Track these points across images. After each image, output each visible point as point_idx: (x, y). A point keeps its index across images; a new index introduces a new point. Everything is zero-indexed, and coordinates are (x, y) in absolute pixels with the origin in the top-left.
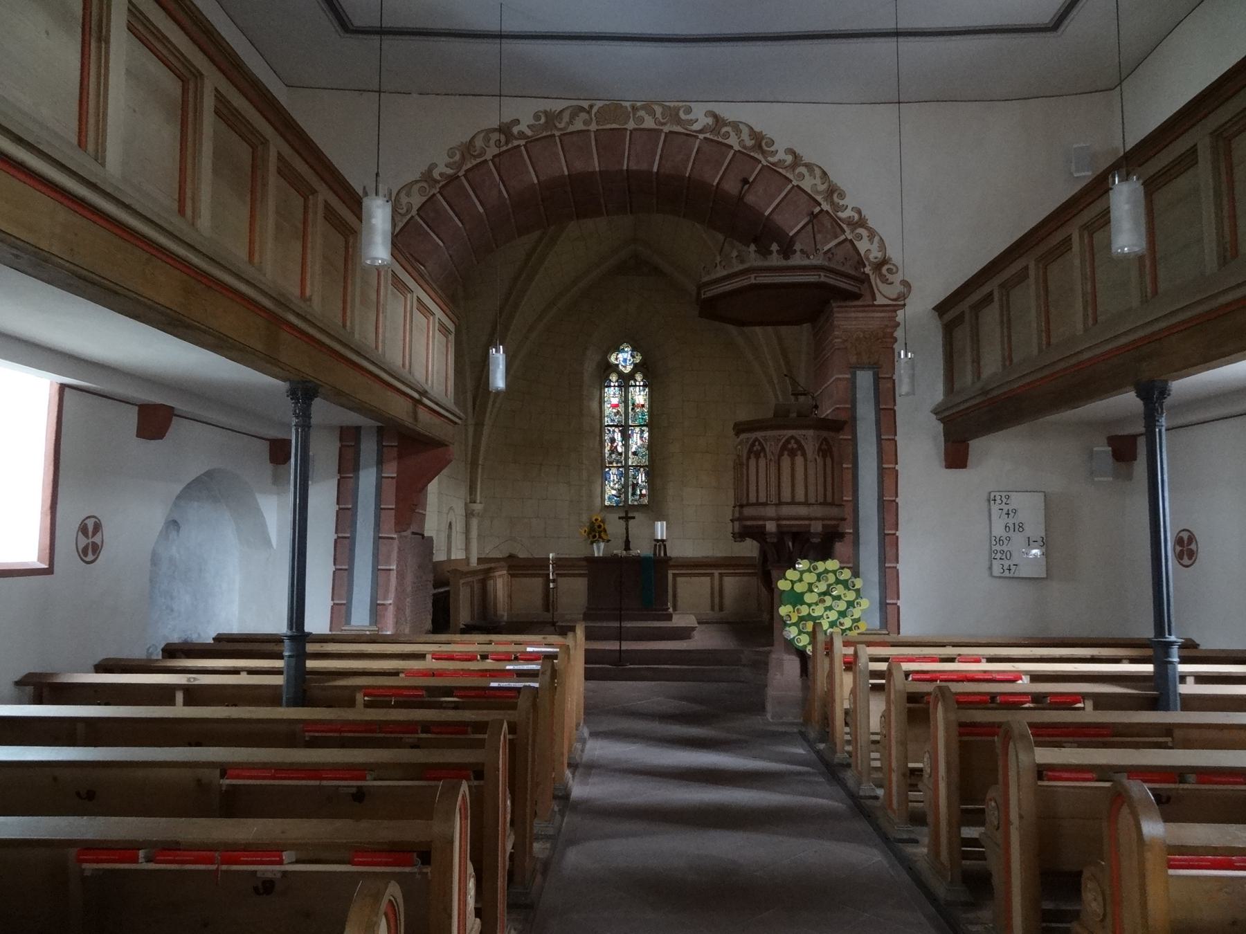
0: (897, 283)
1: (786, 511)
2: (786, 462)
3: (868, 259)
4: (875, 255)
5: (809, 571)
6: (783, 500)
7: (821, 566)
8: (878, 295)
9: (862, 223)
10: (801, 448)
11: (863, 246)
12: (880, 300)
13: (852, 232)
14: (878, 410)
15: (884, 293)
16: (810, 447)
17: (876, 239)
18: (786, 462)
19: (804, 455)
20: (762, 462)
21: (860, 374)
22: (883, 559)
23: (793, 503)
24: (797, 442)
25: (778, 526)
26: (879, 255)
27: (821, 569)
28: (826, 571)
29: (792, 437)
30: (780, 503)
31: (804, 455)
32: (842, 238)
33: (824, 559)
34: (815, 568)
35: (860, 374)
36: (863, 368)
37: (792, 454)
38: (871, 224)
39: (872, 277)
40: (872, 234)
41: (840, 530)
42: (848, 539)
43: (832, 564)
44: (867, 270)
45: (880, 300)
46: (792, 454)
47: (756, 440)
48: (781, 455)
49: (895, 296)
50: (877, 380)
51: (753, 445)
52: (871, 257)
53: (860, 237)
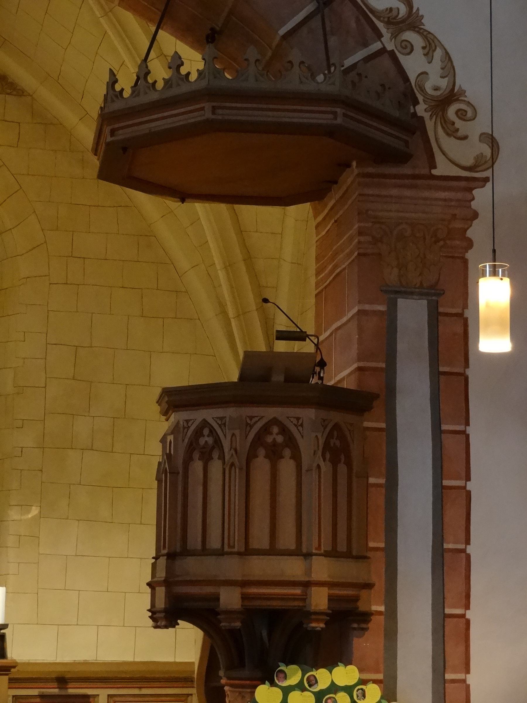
0: (474, 137)
1: (261, 567)
2: (262, 465)
3: (422, 90)
4: (435, 82)
5: (300, 687)
6: (255, 544)
7: (323, 678)
8: (439, 158)
9: (412, 22)
10: (291, 442)
11: (413, 64)
12: (443, 168)
13: (394, 36)
14: (436, 375)
15: (452, 155)
16: (309, 443)
17: (438, 53)
18: (262, 465)
19: (296, 457)
20: (216, 468)
21: (401, 302)
22: (440, 665)
23: (273, 551)
24: (284, 430)
25: (245, 597)
26: (444, 83)
27: (323, 684)
28: (334, 688)
29: (275, 421)
30: (248, 552)
31: (296, 457)
32: (376, 46)
33: (330, 665)
34: (313, 681)
35: (401, 302)
36: (407, 294)
37: (274, 454)
38: (428, 24)
39: (429, 125)
40: (431, 44)
41: (362, 607)
42: (377, 624)
43: (345, 675)
44: (421, 109)
45: (443, 168)
46: (274, 454)
47: (205, 423)
48: (251, 456)
49: (469, 162)
50: (434, 317)
51: (199, 433)
52: (428, 87)
53: (409, 49)
